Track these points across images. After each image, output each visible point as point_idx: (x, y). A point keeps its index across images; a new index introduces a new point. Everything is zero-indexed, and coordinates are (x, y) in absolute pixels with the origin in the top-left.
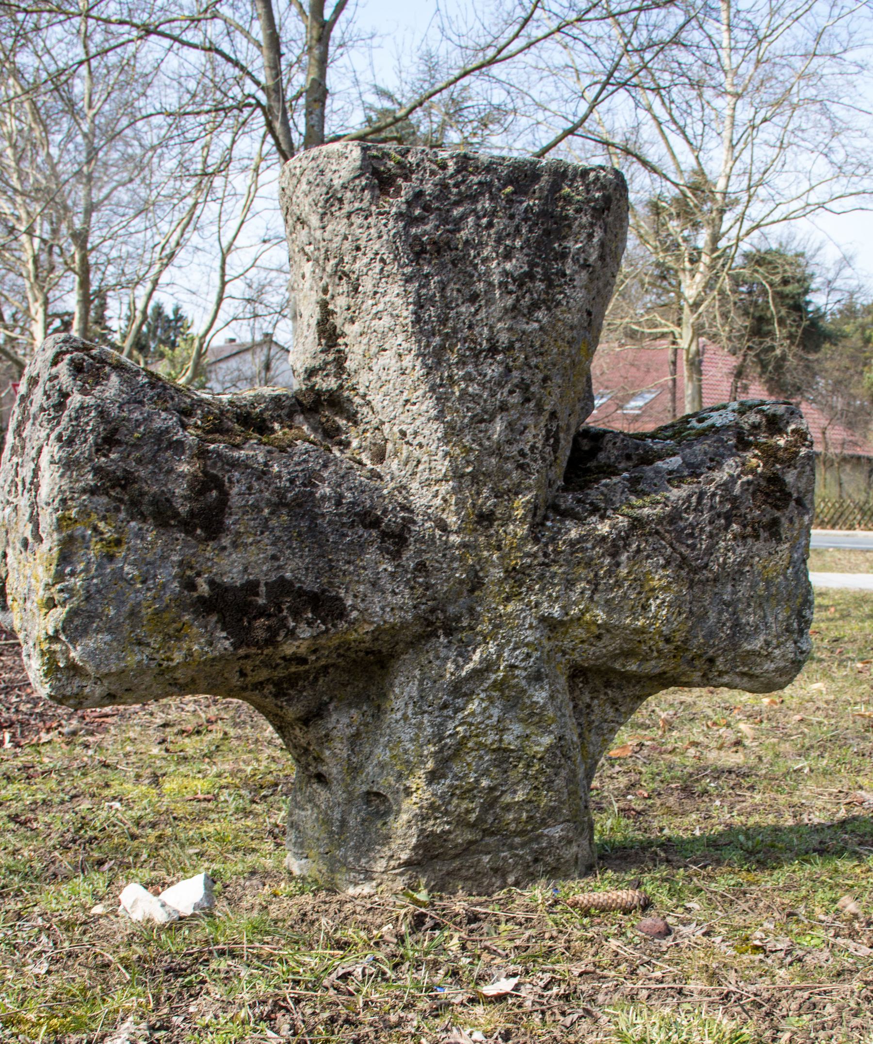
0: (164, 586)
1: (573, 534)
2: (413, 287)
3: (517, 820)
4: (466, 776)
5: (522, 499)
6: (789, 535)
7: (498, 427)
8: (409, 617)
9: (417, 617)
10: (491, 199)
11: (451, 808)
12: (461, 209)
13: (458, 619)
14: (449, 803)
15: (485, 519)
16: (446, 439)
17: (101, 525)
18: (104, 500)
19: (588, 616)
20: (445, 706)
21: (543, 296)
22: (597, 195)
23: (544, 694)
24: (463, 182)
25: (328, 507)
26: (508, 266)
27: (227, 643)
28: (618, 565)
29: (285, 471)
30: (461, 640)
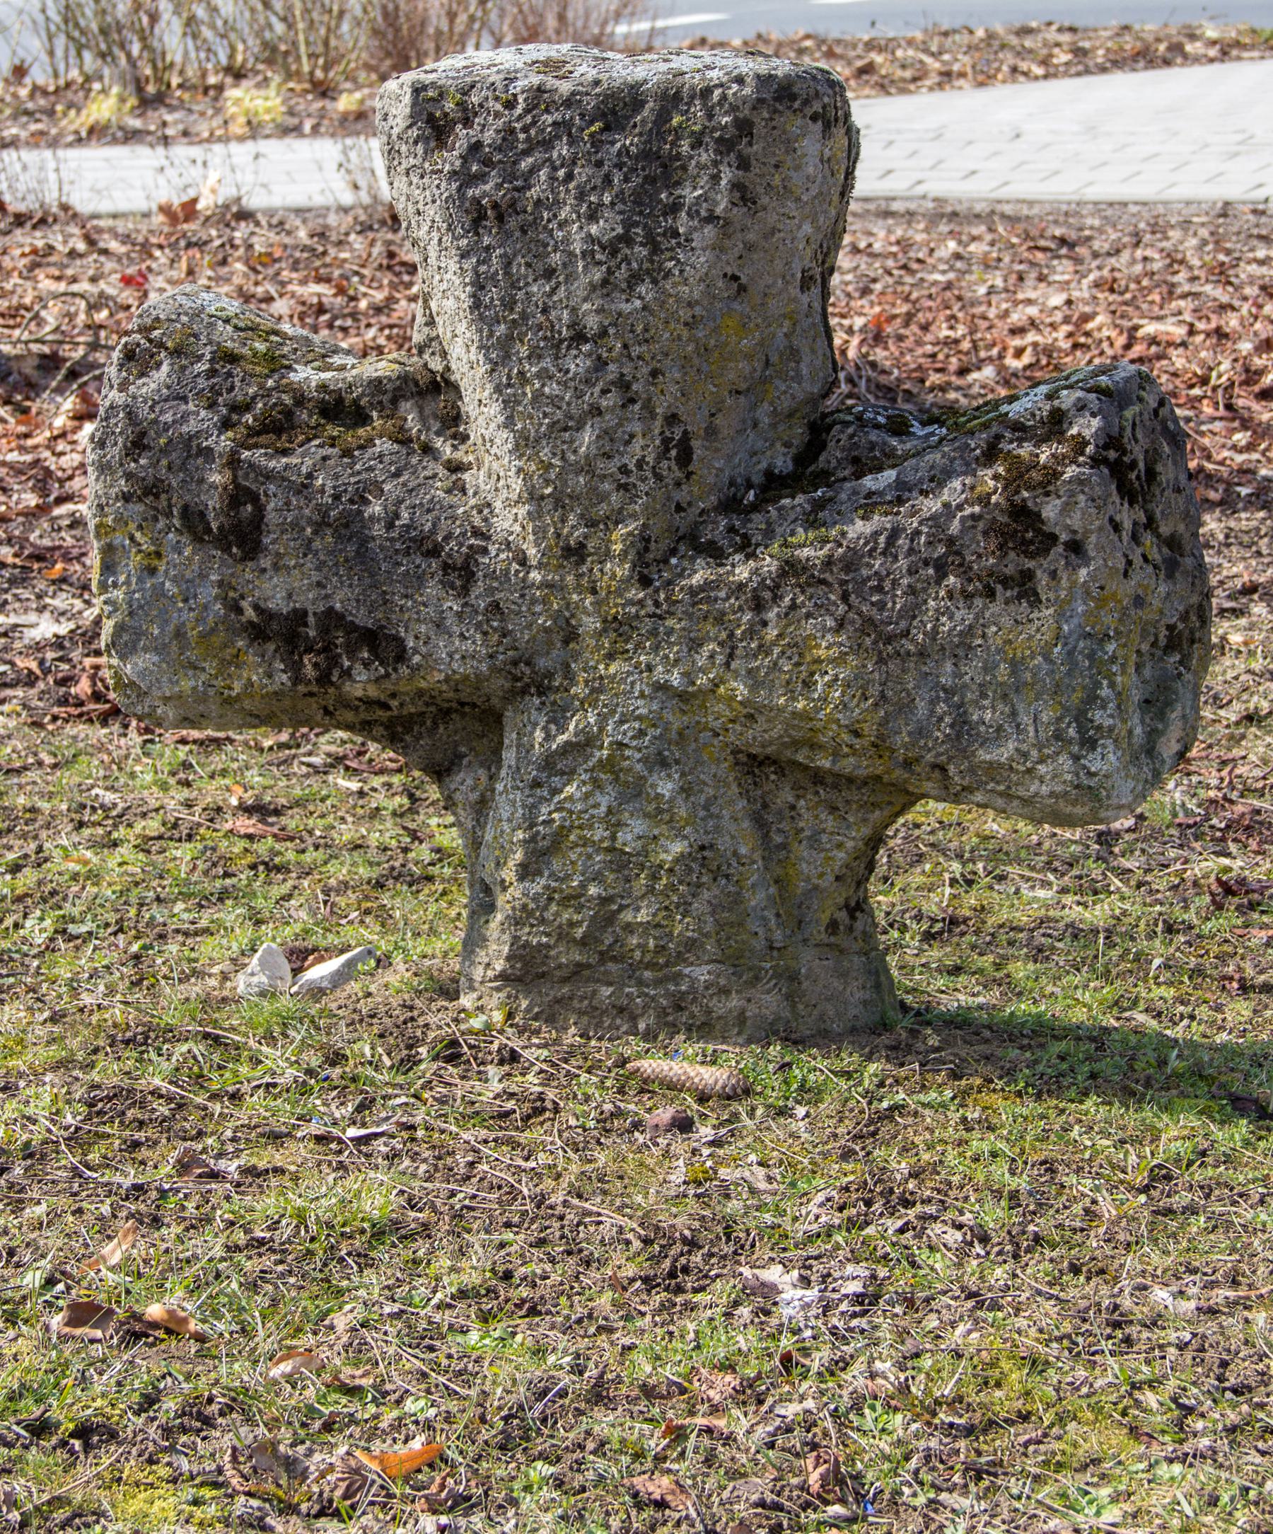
0: (206, 607)
1: (697, 579)
2: (469, 264)
3: (643, 947)
4: (568, 877)
5: (622, 530)
6: (1052, 596)
7: (587, 438)
8: (484, 667)
9: (493, 669)
10: (570, 144)
11: (549, 915)
12: (530, 160)
13: (550, 675)
14: (546, 908)
15: (576, 553)
16: (517, 450)
17: (138, 535)
18: (140, 508)
19: (722, 690)
20: (536, 784)
21: (646, 265)
22: (725, 120)
23: (670, 786)
24: (534, 123)
25: (378, 530)
26: (594, 229)
27: (284, 677)
28: (765, 624)
29: (329, 484)
30: (554, 703)
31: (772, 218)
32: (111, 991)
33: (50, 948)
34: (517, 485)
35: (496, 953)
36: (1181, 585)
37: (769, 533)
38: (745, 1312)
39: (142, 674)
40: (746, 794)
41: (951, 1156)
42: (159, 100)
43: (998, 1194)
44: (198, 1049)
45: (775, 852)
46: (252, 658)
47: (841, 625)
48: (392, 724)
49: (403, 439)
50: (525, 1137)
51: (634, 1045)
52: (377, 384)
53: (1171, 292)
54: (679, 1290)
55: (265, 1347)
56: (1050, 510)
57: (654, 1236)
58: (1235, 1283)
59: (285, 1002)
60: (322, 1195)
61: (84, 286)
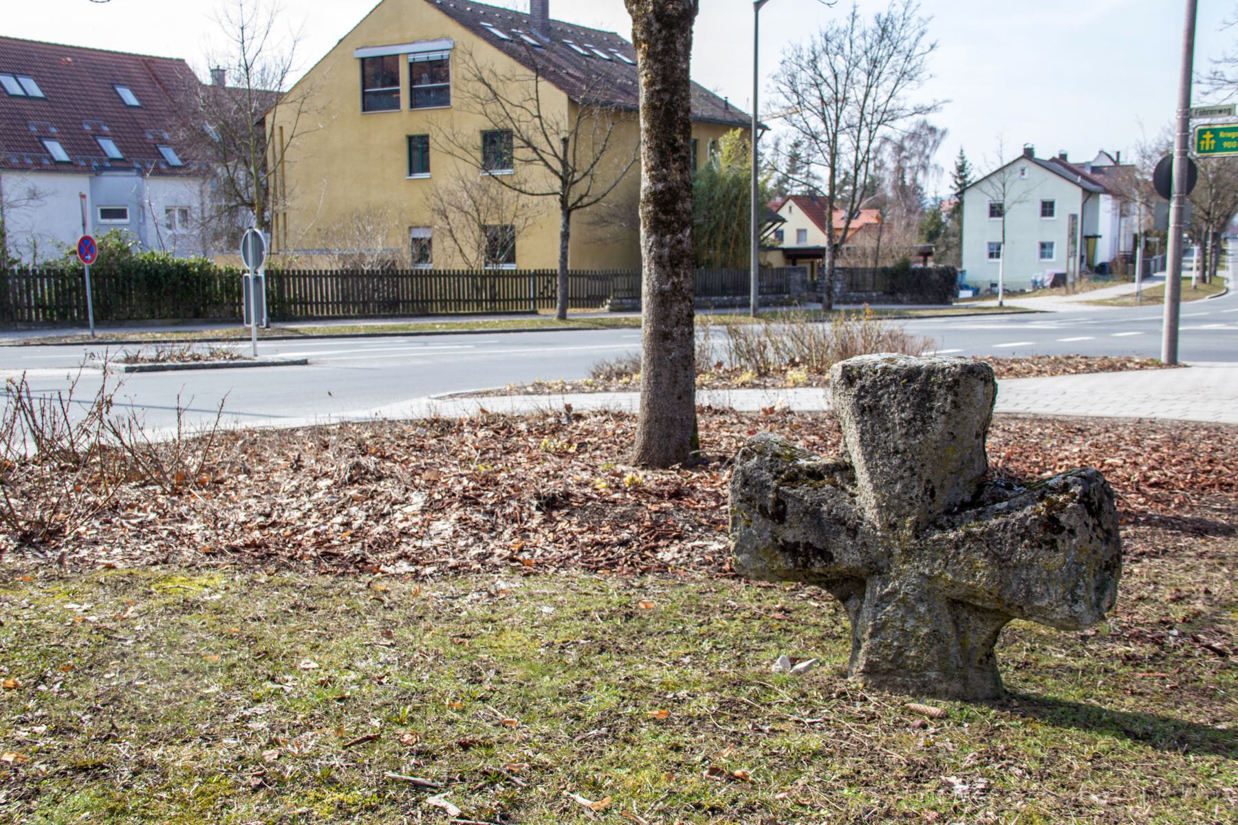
1: (936, 537)
5: (909, 519)
7: (898, 486)
15: (893, 526)
20: (877, 606)
25: (825, 516)
31: (965, 414)
32: (730, 667)
33: (711, 652)
34: (874, 502)
35: (861, 663)
36: (1111, 547)
37: (962, 523)
38: (942, 791)
39: (744, 561)
40: (950, 613)
41: (1020, 744)
42: (765, 374)
43: (1036, 758)
44: (758, 689)
45: (961, 634)
46: (781, 557)
47: (986, 555)
48: (828, 583)
49: (835, 485)
50: (868, 726)
51: (907, 698)
52: (827, 466)
53: (1118, 449)
54: (919, 782)
55: (776, 788)
56: (1063, 518)
57: (910, 762)
58: (1122, 795)
59: (787, 676)
60: (796, 740)
61: (736, 434)
